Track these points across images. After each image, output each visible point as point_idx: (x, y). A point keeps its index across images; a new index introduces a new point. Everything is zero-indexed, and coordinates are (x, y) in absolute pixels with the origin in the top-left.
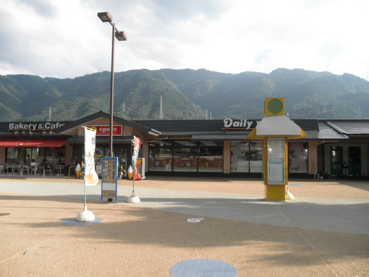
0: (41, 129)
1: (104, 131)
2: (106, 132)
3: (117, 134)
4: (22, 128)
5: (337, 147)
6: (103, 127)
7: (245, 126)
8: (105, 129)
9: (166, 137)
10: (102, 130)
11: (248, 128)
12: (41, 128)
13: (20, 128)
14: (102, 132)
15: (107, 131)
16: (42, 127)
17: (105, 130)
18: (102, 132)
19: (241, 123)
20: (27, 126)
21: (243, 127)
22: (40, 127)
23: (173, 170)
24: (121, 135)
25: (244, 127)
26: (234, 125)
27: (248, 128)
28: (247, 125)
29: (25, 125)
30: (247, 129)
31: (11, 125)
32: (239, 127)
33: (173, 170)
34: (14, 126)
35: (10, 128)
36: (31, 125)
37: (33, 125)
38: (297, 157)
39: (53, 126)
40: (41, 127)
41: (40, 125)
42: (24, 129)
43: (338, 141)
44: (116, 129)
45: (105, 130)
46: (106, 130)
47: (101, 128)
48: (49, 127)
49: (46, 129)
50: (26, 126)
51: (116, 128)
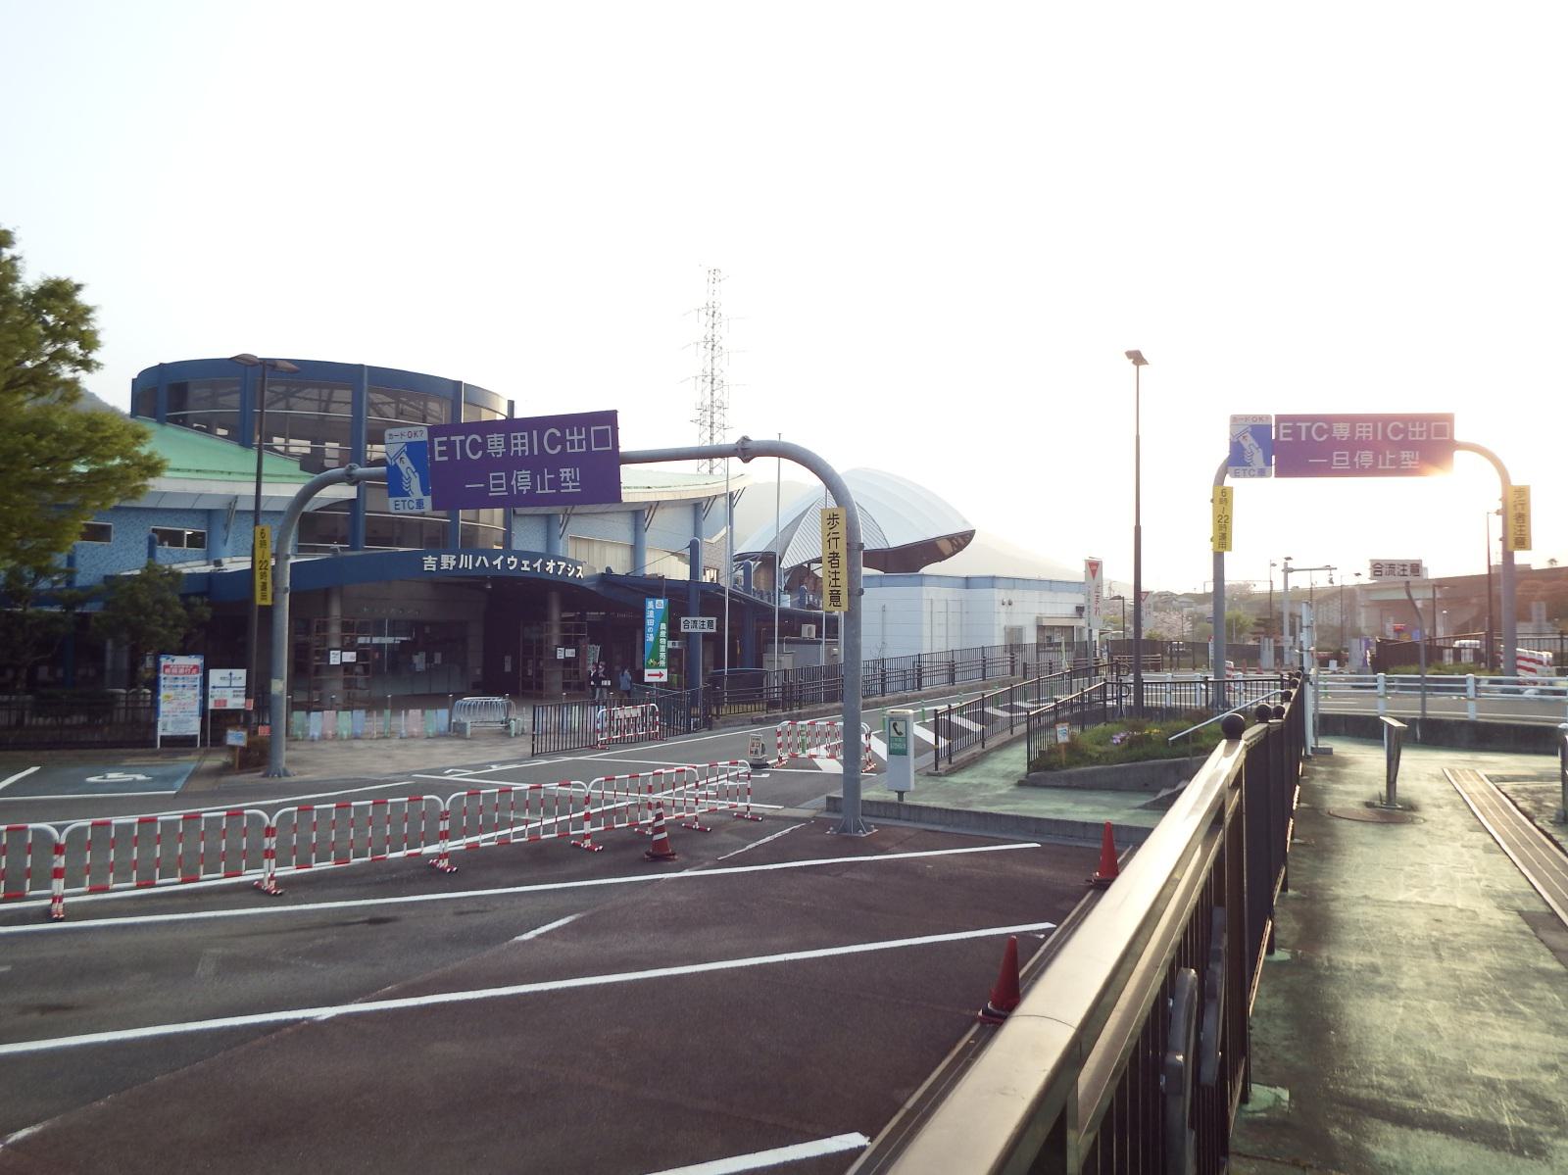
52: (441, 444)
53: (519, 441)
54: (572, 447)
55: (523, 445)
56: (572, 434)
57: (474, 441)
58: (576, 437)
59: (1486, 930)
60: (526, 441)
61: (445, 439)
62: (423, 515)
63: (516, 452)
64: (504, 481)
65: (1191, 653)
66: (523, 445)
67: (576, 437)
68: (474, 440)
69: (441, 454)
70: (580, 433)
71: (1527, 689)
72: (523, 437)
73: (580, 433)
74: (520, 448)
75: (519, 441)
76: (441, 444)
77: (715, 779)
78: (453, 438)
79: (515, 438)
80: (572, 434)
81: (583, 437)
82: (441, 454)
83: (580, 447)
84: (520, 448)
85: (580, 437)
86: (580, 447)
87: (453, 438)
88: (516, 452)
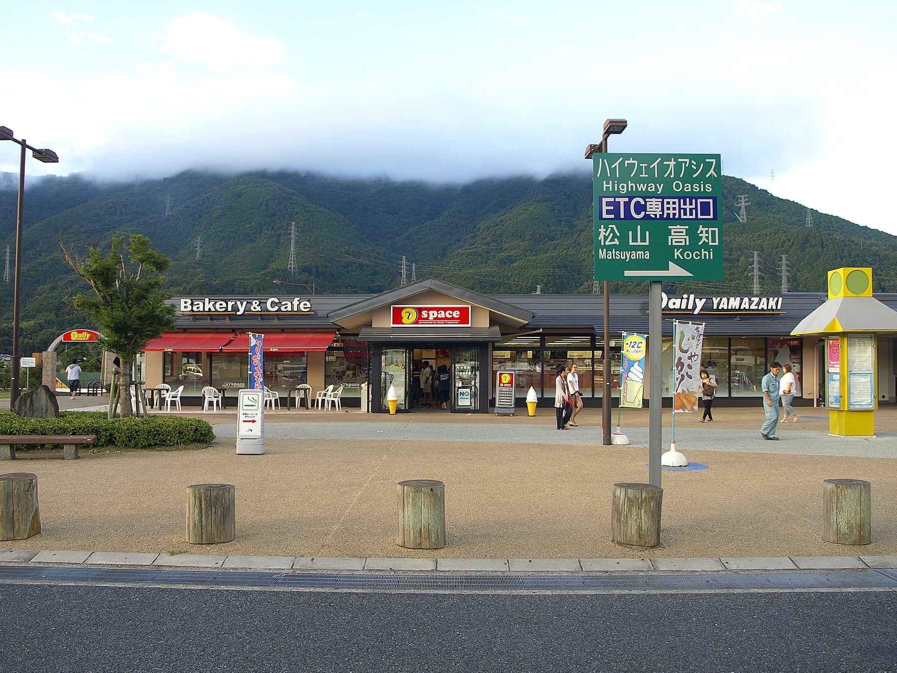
0: (258, 311)
1: (431, 318)
2: (437, 318)
3: (460, 323)
4: (213, 309)
5: (210, 488)
6: (429, 309)
7: (690, 307)
8: (435, 312)
9: (539, 329)
10: (428, 314)
11: (696, 312)
12: (259, 309)
13: (207, 309)
14: (427, 319)
15: (439, 316)
16: (260, 307)
17: (433, 315)
18: (427, 319)
19: (685, 301)
20: (224, 305)
21: (686, 309)
22: (254, 308)
23: (593, 395)
24: (469, 325)
25: (690, 310)
26: (671, 306)
27: (696, 312)
28: (695, 306)
29: (455, 312)
30: (694, 313)
31: (186, 303)
32: (680, 309)
33: (593, 395)
34: (192, 304)
35: (183, 309)
36: (234, 303)
37: (239, 303)
38: (403, 484)
39: (286, 304)
40: (256, 307)
41: (256, 303)
42: (216, 311)
43: (433, 344)
44: (458, 313)
45: (433, 315)
46: (435, 316)
47: (427, 312)
48: (276, 308)
49: (270, 311)
50: (221, 304)
51: (458, 312)
52: (608, 204)
53: (671, 206)
54: (685, 214)
55: (674, 209)
56: (685, 204)
57: (638, 203)
58: (688, 207)
59: (211, 445)
60: (671, 201)
61: (612, 200)
62: (287, 311)
63: (668, 214)
64: (639, 243)
65: (269, 360)
66: (674, 209)
67: (688, 207)
68: (638, 202)
69: (608, 212)
70: (691, 204)
71: (71, 332)
72: (668, 203)
73: (691, 204)
74: (671, 212)
75: (671, 206)
76: (608, 204)
77: (92, 389)
78: (617, 200)
79: (674, 203)
80: (685, 204)
81: (693, 206)
82: (608, 212)
83: (691, 214)
84: (671, 212)
85: (691, 207)
86: (691, 214)
87: (617, 200)
88: (668, 214)
